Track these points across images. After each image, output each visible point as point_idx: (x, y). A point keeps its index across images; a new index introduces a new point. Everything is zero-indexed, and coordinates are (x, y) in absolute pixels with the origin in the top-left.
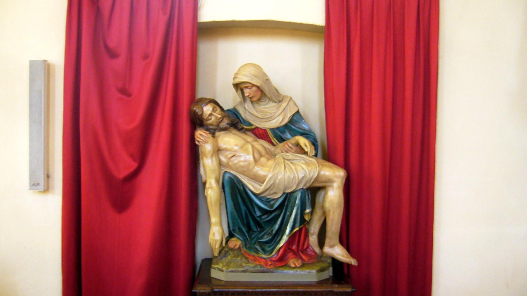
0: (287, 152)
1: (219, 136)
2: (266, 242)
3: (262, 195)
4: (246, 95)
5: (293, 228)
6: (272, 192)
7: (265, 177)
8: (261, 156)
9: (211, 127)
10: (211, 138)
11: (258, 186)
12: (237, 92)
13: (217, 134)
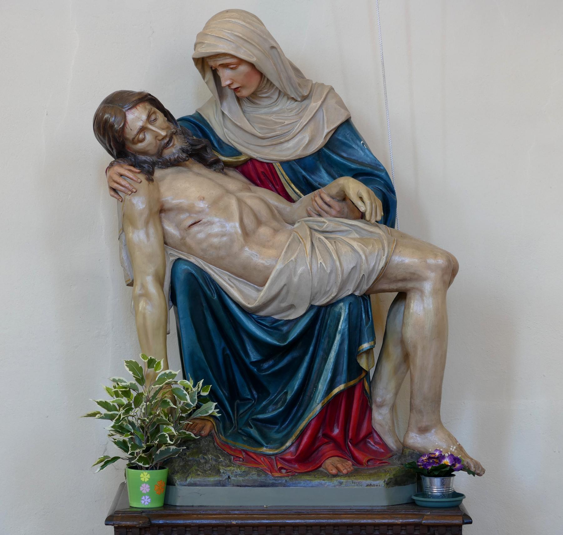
0: (320, 215)
1: (163, 178)
2: (272, 421)
3: (262, 313)
4: (225, 82)
5: (332, 385)
6: (284, 305)
7: (269, 269)
8: (259, 222)
9: (143, 158)
10: (145, 182)
11: (250, 291)
12: (204, 78)
13: (158, 173)
